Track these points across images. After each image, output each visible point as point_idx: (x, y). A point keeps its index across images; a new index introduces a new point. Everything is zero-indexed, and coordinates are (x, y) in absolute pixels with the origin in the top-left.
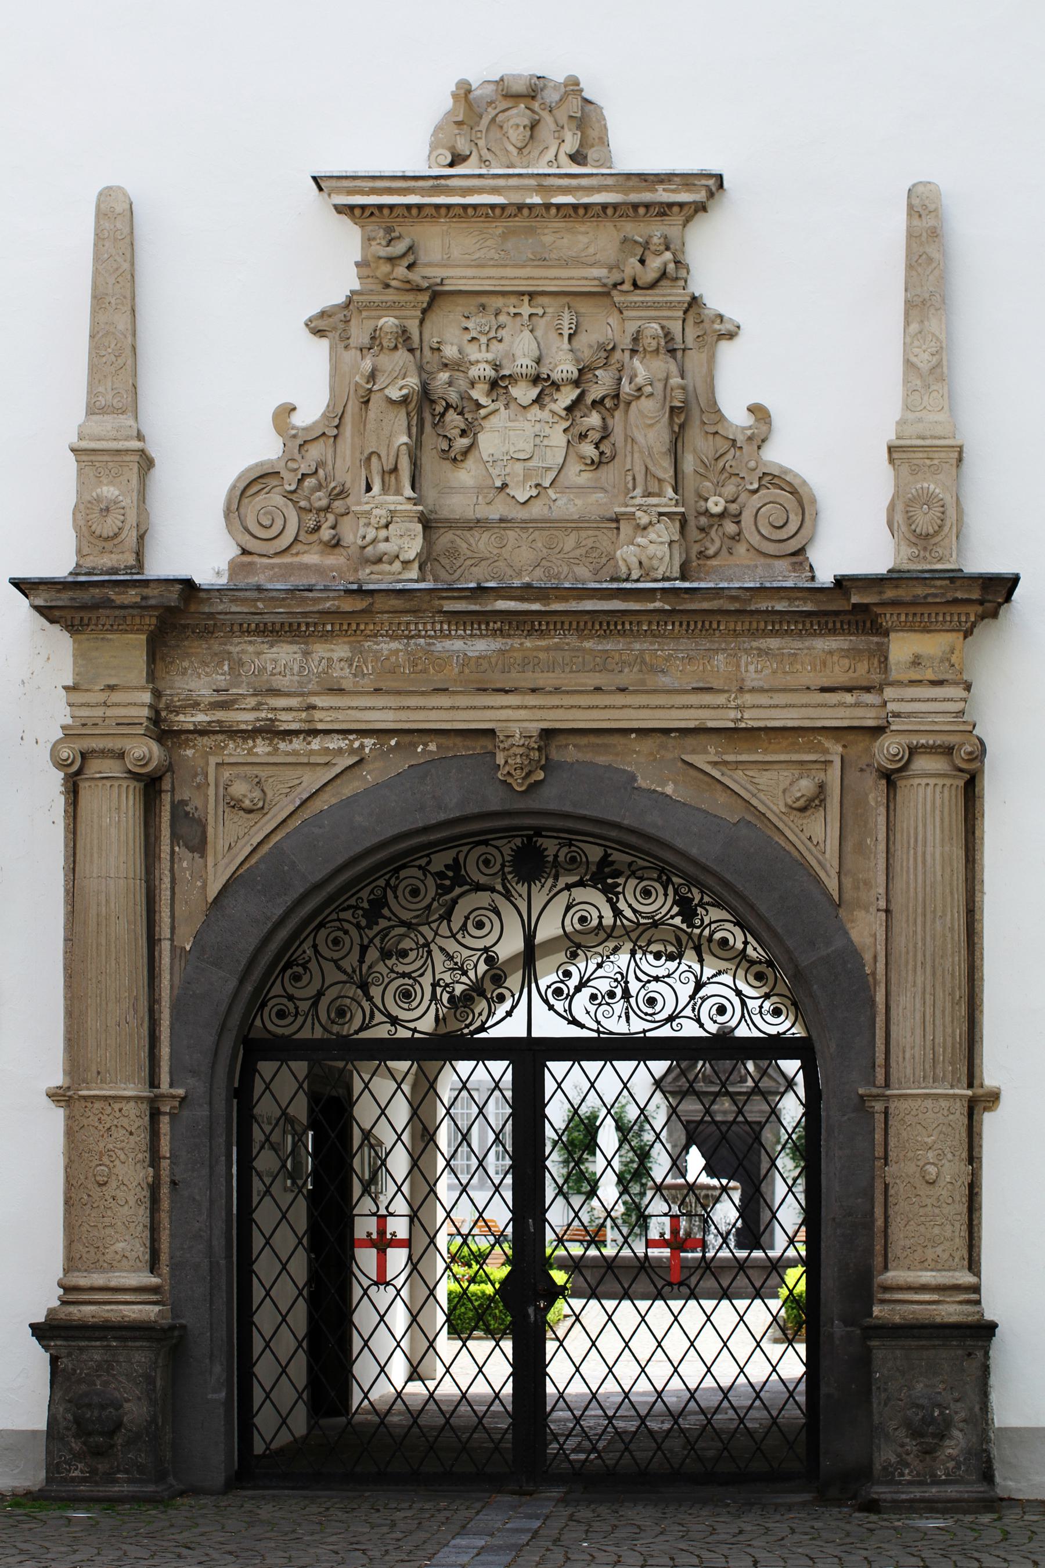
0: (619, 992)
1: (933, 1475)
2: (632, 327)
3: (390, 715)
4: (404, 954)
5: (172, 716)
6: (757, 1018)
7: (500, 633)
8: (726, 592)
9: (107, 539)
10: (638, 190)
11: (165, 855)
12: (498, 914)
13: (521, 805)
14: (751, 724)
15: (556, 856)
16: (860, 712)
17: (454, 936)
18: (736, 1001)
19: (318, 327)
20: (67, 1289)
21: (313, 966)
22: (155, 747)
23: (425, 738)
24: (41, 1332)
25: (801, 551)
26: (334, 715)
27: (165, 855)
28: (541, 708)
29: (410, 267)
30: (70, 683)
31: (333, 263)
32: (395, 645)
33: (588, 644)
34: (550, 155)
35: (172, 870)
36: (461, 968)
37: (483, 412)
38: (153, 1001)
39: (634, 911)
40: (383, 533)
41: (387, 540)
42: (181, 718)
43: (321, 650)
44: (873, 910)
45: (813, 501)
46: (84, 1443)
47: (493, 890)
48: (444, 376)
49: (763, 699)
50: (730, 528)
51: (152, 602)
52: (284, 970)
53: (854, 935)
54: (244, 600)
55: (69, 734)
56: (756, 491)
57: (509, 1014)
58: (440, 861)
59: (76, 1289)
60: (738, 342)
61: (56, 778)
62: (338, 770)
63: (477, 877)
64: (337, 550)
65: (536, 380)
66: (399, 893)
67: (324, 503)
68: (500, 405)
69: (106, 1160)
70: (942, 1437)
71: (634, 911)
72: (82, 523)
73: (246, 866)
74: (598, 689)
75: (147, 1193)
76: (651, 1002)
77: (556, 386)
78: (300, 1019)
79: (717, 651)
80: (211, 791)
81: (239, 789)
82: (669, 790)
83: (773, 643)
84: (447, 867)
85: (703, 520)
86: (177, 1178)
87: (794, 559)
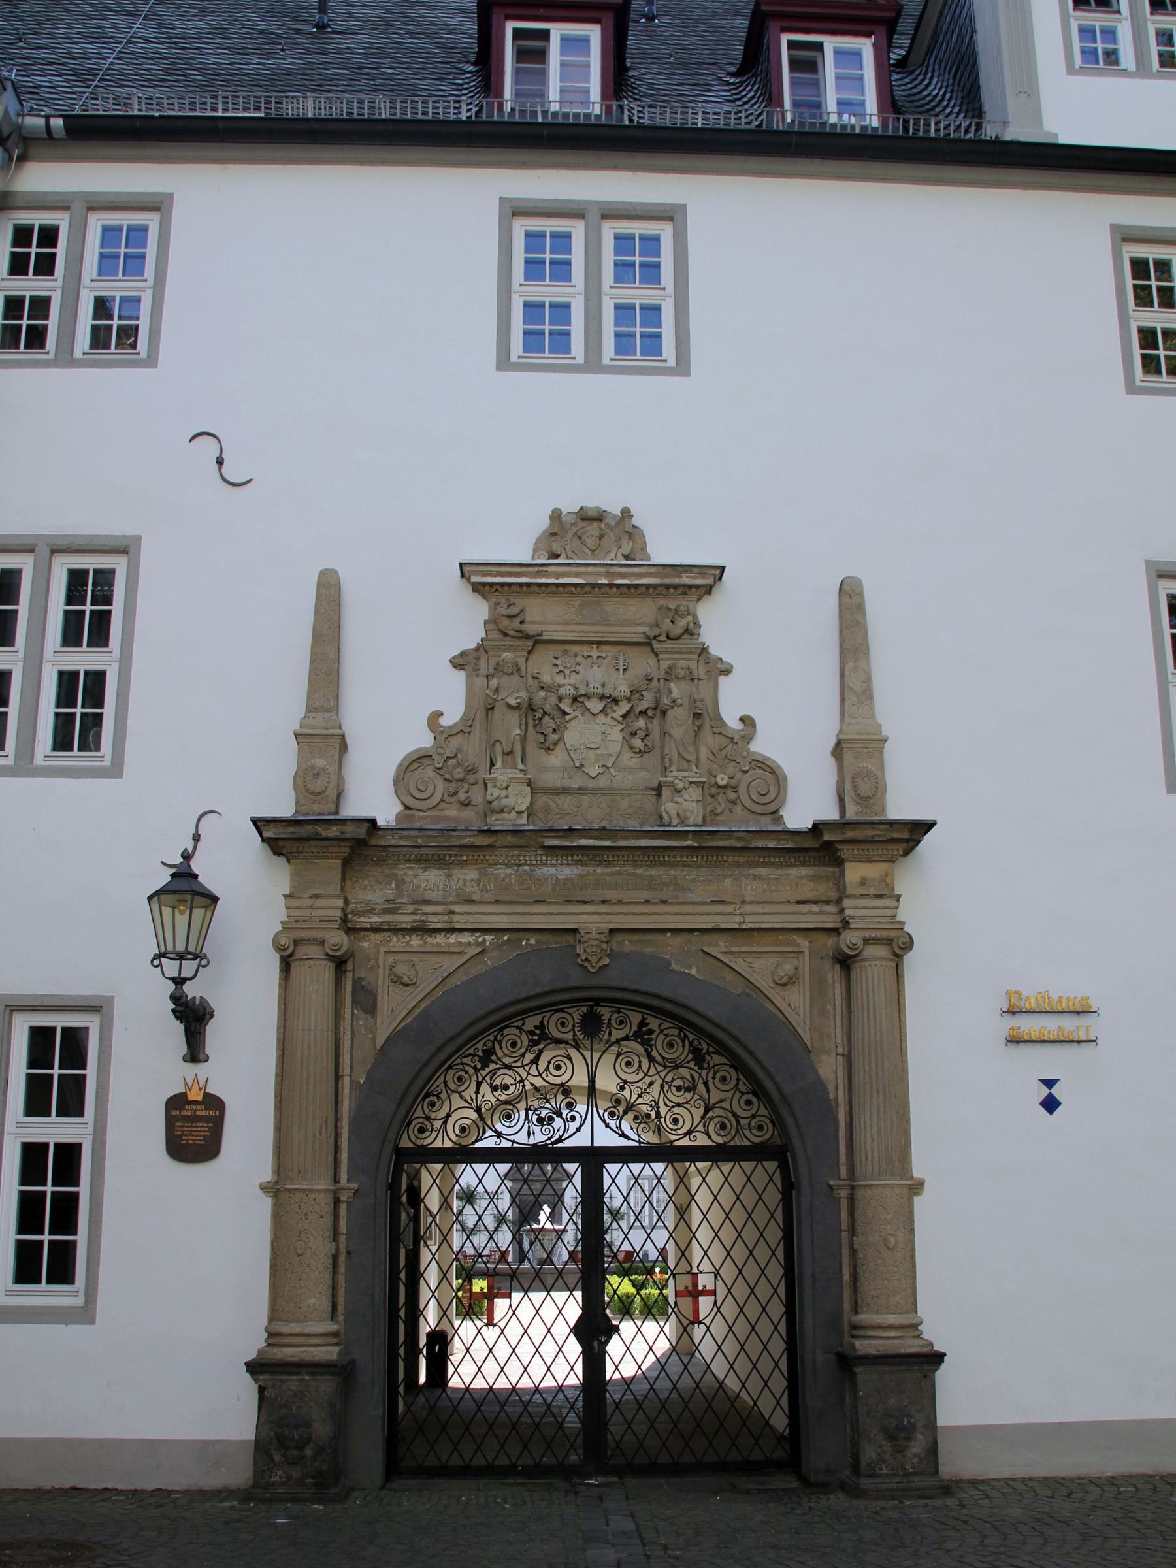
0: (653, 1114)
1: (904, 1469)
2: (665, 665)
3: (505, 918)
4: (506, 1087)
5: (355, 918)
6: (747, 1132)
7: (581, 863)
8: (736, 835)
9: (316, 794)
10: (667, 576)
11: (348, 1015)
12: (570, 1059)
13: (593, 982)
14: (750, 926)
15: (610, 1020)
16: (822, 918)
17: (540, 1075)
18: (733, 1120)
19: (458, 663)
20: (271, 1335)
21: (444, 1095)
22: (345, 937)
23: (528, 935)
24: (254, 1368)
25: (777, 811)
26: (466, 918)
27: (348, 1015)
28: (608, 914)
29: (522, 622)
30: (288, 892)
31: (469, 623)
32: (509, 871)
33: (639, 871)
34: (613, 555)
35: (352, 1026)
36: (545, 1098)
37: (568, 717)
38: (337, 1120)
39: (663, 1058)
40: (504, 793)
41: (507, 797)
42: (362, 919)
43: (458, 873)
44: (833, 1054)
45: (786, 779)
46: (284, 1455)
47: (567, 1043)
48: (542, 694)
49: (758, 909)
50: (732, 796)
51: (348, 836)
52: (424, 1098)
53: (821, 1072)
54: (408, 837)
55: (286, 927)
56: (746, 772)
57: (578, 1130)
58: (531, 1023)
59: (279, 1335)
60: (731, 676)
61: (274, 960)
62: (468, 956)
63: (556, 1034)
64: (469, 808)
65: (602, 698)
66: (503, 1044)
67: (461, 776)
68: (578, 713)
69: (303, 1236)
70: (909, 1439)
71: (663, 1058)
72: (300, 783)
73: (404, 1024)
74: (647, 901)
75: (330, 1261)
76: (675, 1121)
77: (616, 701)
78: (434, 1134)
79: (725, 876)
80: (381, 971)
81: (401, 969)
82: (693, 972)
83: (763, 871)
84: (536, 1027)
85: (714, 790)
86: (350, 1249)
87: (773, 816)
